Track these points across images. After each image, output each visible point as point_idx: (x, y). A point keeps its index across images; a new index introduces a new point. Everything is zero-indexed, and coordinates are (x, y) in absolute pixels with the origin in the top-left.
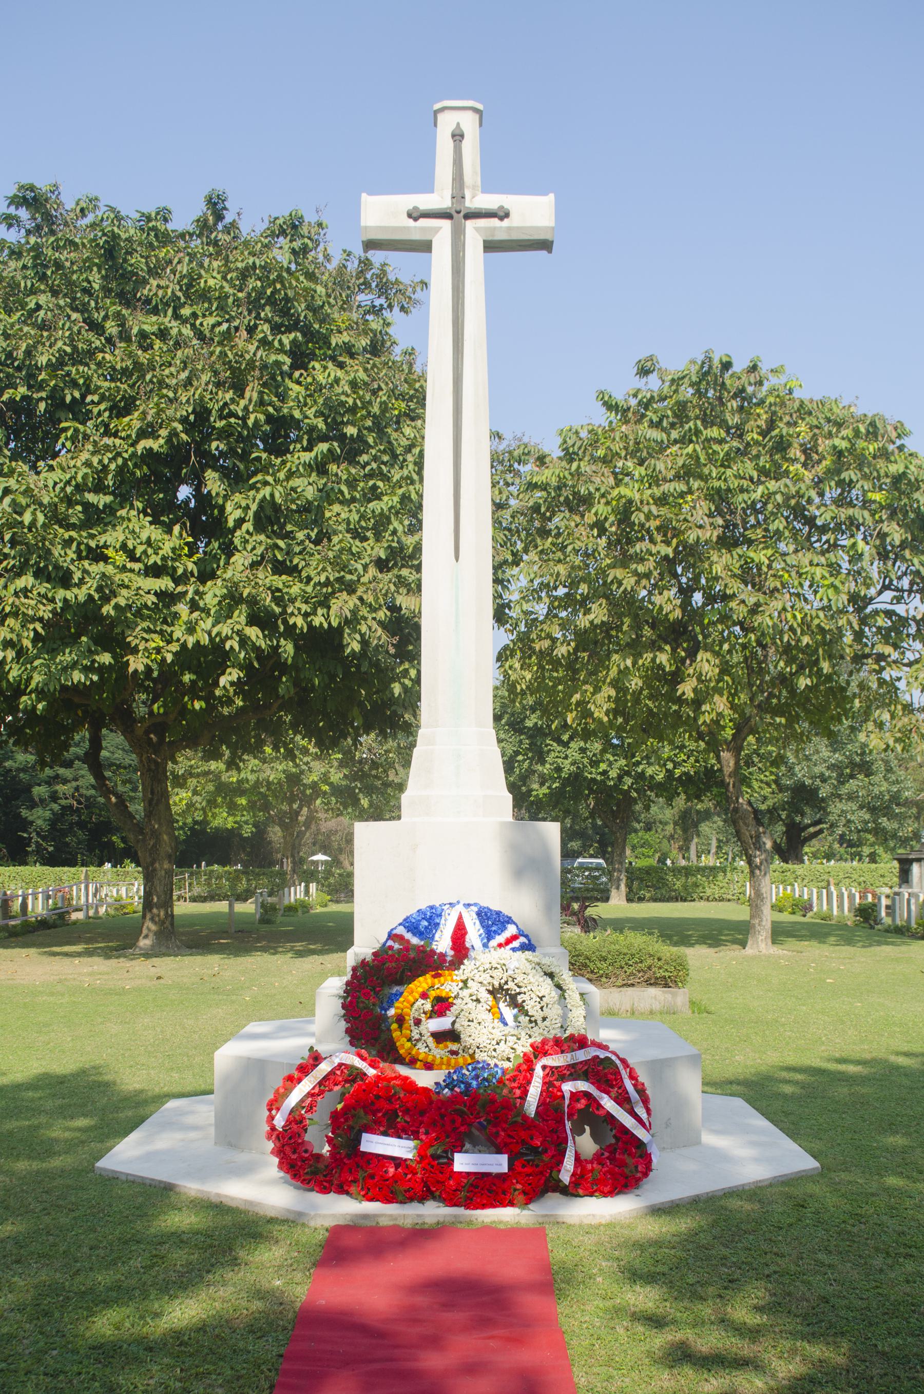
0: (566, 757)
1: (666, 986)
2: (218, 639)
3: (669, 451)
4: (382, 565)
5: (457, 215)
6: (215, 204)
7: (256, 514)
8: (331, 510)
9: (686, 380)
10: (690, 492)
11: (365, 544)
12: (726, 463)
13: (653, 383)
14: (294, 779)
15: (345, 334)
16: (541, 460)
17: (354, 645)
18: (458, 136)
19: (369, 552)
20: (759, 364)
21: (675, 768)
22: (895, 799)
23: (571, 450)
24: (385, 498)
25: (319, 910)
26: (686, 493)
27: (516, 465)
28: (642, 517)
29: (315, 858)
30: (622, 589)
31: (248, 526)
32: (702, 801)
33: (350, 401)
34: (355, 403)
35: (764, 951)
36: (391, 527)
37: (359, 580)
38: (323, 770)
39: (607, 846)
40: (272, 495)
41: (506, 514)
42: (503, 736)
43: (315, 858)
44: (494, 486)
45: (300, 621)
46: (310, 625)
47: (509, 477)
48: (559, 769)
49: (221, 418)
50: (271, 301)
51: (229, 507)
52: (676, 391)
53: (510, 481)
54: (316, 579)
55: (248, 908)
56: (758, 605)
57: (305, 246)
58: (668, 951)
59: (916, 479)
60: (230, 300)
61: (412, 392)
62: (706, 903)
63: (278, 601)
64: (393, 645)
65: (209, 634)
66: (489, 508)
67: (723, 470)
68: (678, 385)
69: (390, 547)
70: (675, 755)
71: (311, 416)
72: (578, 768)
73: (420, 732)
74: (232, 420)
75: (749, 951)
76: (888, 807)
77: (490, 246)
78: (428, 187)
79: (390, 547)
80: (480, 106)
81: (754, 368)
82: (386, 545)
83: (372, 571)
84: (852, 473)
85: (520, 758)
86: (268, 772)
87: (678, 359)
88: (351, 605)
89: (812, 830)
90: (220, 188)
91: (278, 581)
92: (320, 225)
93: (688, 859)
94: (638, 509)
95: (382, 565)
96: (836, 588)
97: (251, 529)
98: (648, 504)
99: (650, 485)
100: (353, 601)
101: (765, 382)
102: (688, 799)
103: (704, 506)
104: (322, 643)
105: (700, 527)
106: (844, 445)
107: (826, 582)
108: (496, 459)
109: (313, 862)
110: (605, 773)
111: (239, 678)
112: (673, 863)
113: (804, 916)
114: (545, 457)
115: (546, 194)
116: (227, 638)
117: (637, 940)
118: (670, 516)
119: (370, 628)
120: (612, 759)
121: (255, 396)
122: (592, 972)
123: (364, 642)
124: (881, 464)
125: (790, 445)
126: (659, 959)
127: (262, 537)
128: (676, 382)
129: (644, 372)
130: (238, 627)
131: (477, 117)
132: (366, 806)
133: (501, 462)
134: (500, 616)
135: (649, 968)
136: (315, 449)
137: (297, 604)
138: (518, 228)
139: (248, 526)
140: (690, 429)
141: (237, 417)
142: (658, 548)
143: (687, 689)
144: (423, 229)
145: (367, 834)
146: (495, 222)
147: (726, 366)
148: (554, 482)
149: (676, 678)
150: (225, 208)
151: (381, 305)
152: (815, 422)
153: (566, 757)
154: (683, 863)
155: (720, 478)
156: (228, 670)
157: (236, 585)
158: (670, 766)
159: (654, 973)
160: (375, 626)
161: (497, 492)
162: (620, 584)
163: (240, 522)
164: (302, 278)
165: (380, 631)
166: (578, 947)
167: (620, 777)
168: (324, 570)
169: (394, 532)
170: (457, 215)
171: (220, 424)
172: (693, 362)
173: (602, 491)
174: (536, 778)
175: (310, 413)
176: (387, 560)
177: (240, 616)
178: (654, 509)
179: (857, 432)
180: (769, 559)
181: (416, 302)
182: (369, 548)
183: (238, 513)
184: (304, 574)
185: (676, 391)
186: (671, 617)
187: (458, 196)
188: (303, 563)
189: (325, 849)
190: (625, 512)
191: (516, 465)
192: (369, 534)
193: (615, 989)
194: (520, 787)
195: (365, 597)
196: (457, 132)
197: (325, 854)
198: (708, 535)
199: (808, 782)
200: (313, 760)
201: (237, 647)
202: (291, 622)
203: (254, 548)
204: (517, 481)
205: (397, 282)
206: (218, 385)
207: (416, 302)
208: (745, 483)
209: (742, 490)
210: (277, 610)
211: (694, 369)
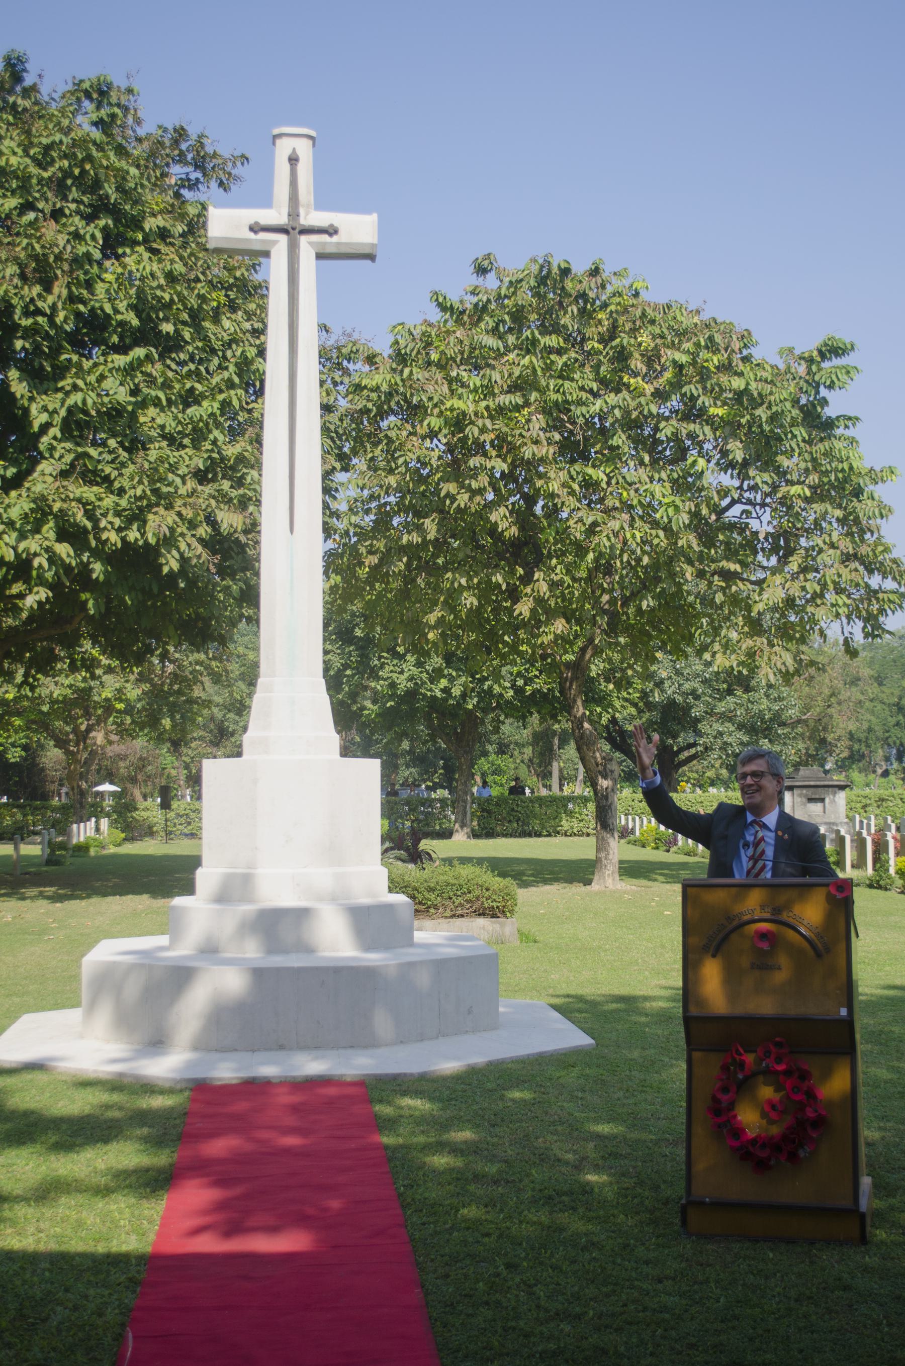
0: (402, 673)
1: (494, 916)
2: (24, 556)
3: (506, 358)
4: (201, 476)
5: (292, 230)
6: (14, 65)
7: (65, 420)
8: (145, 415)
9: (524, 283)
10: (527, 404)
11: (182, 453)
12: (565, 374)
13: (491, 282)
14: (83, 697)
15: (159, 217)
16: (371, 360)
17: (171, 563)
18: (293, 160)
19: (187, 463)
20: (601, 266)
21: (526, 684)
22: (777, 719)
23: (403, 352)
24: (205, 404)
25: (112, 850)
26: (523, 407)
27: (345, 363)
28: (476, 431)
29: (101, 788)
30: (455, 505)
31: (55, 431)
32: (559, 722)
33: (167, 297)
34: (172, 300)
35: (611, 887)
36: (211, 437)
37: (176, 492)
38: (117, 685)
39: (453, 772)
40: (84, 402)
41: (334, 418)
42: (330, 647)
43: (101, 788)
44: (321, 386)
45: (113, 537)
46: (123, 540)
47: (337, 376)
48: (393, 685)
49: (26, 314)
50: (79, 181)
51: (34, 409)
52: (514, 293)
53: (338, 379)
54: (131, 492)
55: (32, 850)
56: (595, 524)
57: (113, 116)
58: (497, 882)
59: (760, 394)
60: (34, 181)
61: (231, 281)
62: (564, 839)
63: (90, 515)
64: (214, 564)
65: (15, 548)
66: (318, 411)
67: (561, 382)
68: (516, 288)
69: (210, 457)
70: (526, 670)
71: (123, 310)
72: (416, 684)
73: (260, 681)
74: (40, 319)
75: (595, 887)
76: (768, 729)
77: (320, 256)
78: (267, 202)
79: (210, 457)
80: (313, 133)
81: (595, 272)
82: (206, 456)
83: (191, 484)
84: (692, 387)
85: (348, 672)
86: (52, 687)
87: (516, 260)
88: (170, 521)
89: (686, 754)
90: (20, 49)
91: (89, 493)
92: (130, 91)
93: (549, 788)
94: (472, 423)
95: (201, 476)
96: (677, 508)
97: (59, 435)
98: (483, 417)
99: (485, 395)
100: (171, 518)
101: (608, 286)
102: (542, 720)
103: (538, 422)
104: (136, 561)
105: (536, 442)
106: (683, 358)
107: (666, 500)
108: (324, 355)
109: (98, 793)
110: (446, 690)
111: (47, 598)
112: (532, 792)
113: (668, 851)
114: (374, 356)
115: (369, 212)
116: (36, 555)
117: (466, 871)
118: (505, 429)
119: (189, 545)
120: (454, 674)
121: (65, 292)
122: (420, 903)
123: (183, 560)
124: (724, 379)
125: (630, 355)
126: (487, 889)
127: (69, 445)
128: (515, 284)
129: (481, 271)
130: (47, 543)
131: (311, 142)
132: (168, 727)
133: (329, 359)
134: (328, 531)
135: (478, 898)
136: (131, 354)
137: (110, 518)
138: (346, 244)
139: (55, 431)
140: (527, 338)
141: (44, 314)
142: (493, 463)
143: (524, 608)
144: (263, 241)
145: (214, 770)
146: (325, 238)
147: (565, 272)
148: (385, 387)
149: (514, 595)
150: (25, 70)
151: (197, 179)
152: (658, 331)
153: (402, 672)
154: (544, 792)
155: (558, 391)
156: (36, 589)
157: (43, 498)
158: (520, 682)
159: (483, 903)
160: (195, 543)
161: (324, 394)
162: (453, 499)
163: (45, 428)
164: (112, 154)
165: (200, 549)
166: (406, 878)
167: (464, 695)
168: (140, 482)
169: (214, 442)
170: (292, 230)
171: (27, 322)
172: (534, 261)
173: (436, 400)
174: (368, 693)
175: (122, 306)
176: (207, 470)
177: (49, 530)
178: (488, 423)
179: (697, 345)
180: (607, 475)
181: (237, 178)
182: (187, 458)
183: (44, 418)
184: (117, 485)
185: (514, 293)
186: (507, 534)
187: (294, 214)
188: (116, 473)
189: (110, 777)
190: (458, 423)
191: (345, 363)
192: (186, 441)
193: (443, 920)
194: (349, 706)
195: (184, 512)
196: (294, 156)
197: (112, 783)
198: (544, 451)
199: (679, 699)
200: (104, 673)
201: (46, 565)
202: (104, 537)
203: (62, 457)
204: (346, 380)
205: (215, 155)
206: (23, 277)
207: (237, 178)
208: (584, 395)
209: (580, 403)
210: (89, 525)
211: (535, 269)
